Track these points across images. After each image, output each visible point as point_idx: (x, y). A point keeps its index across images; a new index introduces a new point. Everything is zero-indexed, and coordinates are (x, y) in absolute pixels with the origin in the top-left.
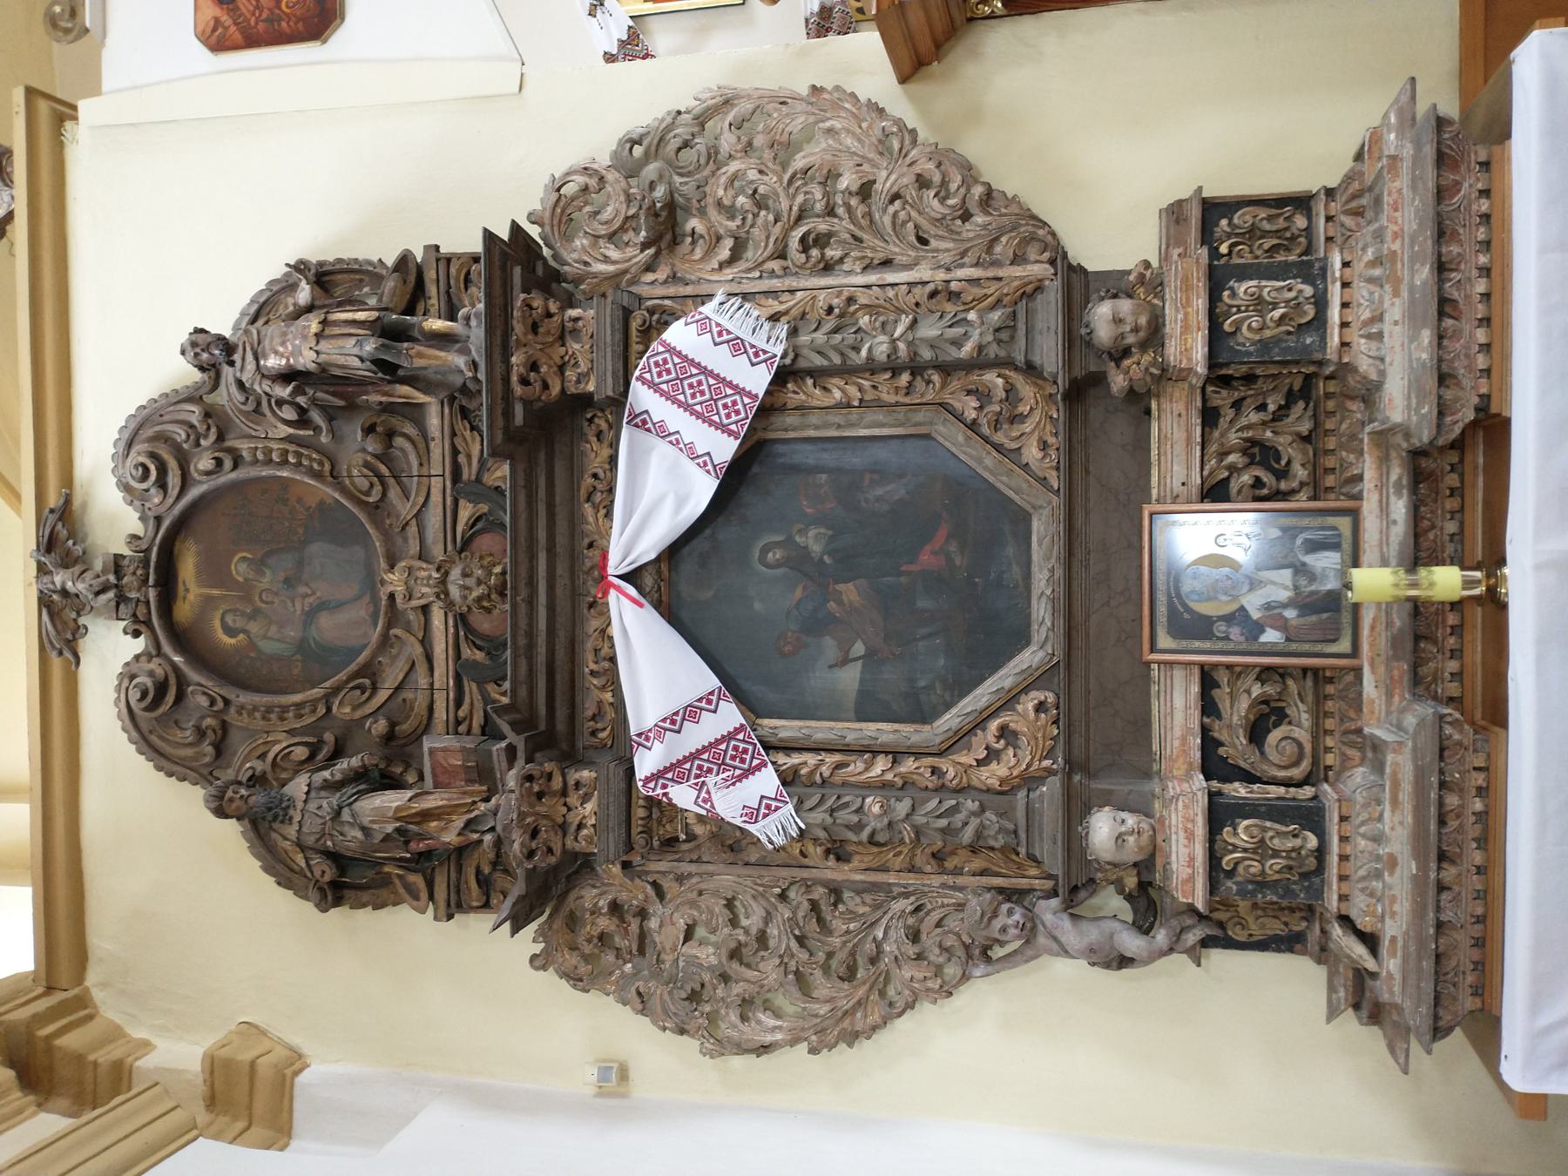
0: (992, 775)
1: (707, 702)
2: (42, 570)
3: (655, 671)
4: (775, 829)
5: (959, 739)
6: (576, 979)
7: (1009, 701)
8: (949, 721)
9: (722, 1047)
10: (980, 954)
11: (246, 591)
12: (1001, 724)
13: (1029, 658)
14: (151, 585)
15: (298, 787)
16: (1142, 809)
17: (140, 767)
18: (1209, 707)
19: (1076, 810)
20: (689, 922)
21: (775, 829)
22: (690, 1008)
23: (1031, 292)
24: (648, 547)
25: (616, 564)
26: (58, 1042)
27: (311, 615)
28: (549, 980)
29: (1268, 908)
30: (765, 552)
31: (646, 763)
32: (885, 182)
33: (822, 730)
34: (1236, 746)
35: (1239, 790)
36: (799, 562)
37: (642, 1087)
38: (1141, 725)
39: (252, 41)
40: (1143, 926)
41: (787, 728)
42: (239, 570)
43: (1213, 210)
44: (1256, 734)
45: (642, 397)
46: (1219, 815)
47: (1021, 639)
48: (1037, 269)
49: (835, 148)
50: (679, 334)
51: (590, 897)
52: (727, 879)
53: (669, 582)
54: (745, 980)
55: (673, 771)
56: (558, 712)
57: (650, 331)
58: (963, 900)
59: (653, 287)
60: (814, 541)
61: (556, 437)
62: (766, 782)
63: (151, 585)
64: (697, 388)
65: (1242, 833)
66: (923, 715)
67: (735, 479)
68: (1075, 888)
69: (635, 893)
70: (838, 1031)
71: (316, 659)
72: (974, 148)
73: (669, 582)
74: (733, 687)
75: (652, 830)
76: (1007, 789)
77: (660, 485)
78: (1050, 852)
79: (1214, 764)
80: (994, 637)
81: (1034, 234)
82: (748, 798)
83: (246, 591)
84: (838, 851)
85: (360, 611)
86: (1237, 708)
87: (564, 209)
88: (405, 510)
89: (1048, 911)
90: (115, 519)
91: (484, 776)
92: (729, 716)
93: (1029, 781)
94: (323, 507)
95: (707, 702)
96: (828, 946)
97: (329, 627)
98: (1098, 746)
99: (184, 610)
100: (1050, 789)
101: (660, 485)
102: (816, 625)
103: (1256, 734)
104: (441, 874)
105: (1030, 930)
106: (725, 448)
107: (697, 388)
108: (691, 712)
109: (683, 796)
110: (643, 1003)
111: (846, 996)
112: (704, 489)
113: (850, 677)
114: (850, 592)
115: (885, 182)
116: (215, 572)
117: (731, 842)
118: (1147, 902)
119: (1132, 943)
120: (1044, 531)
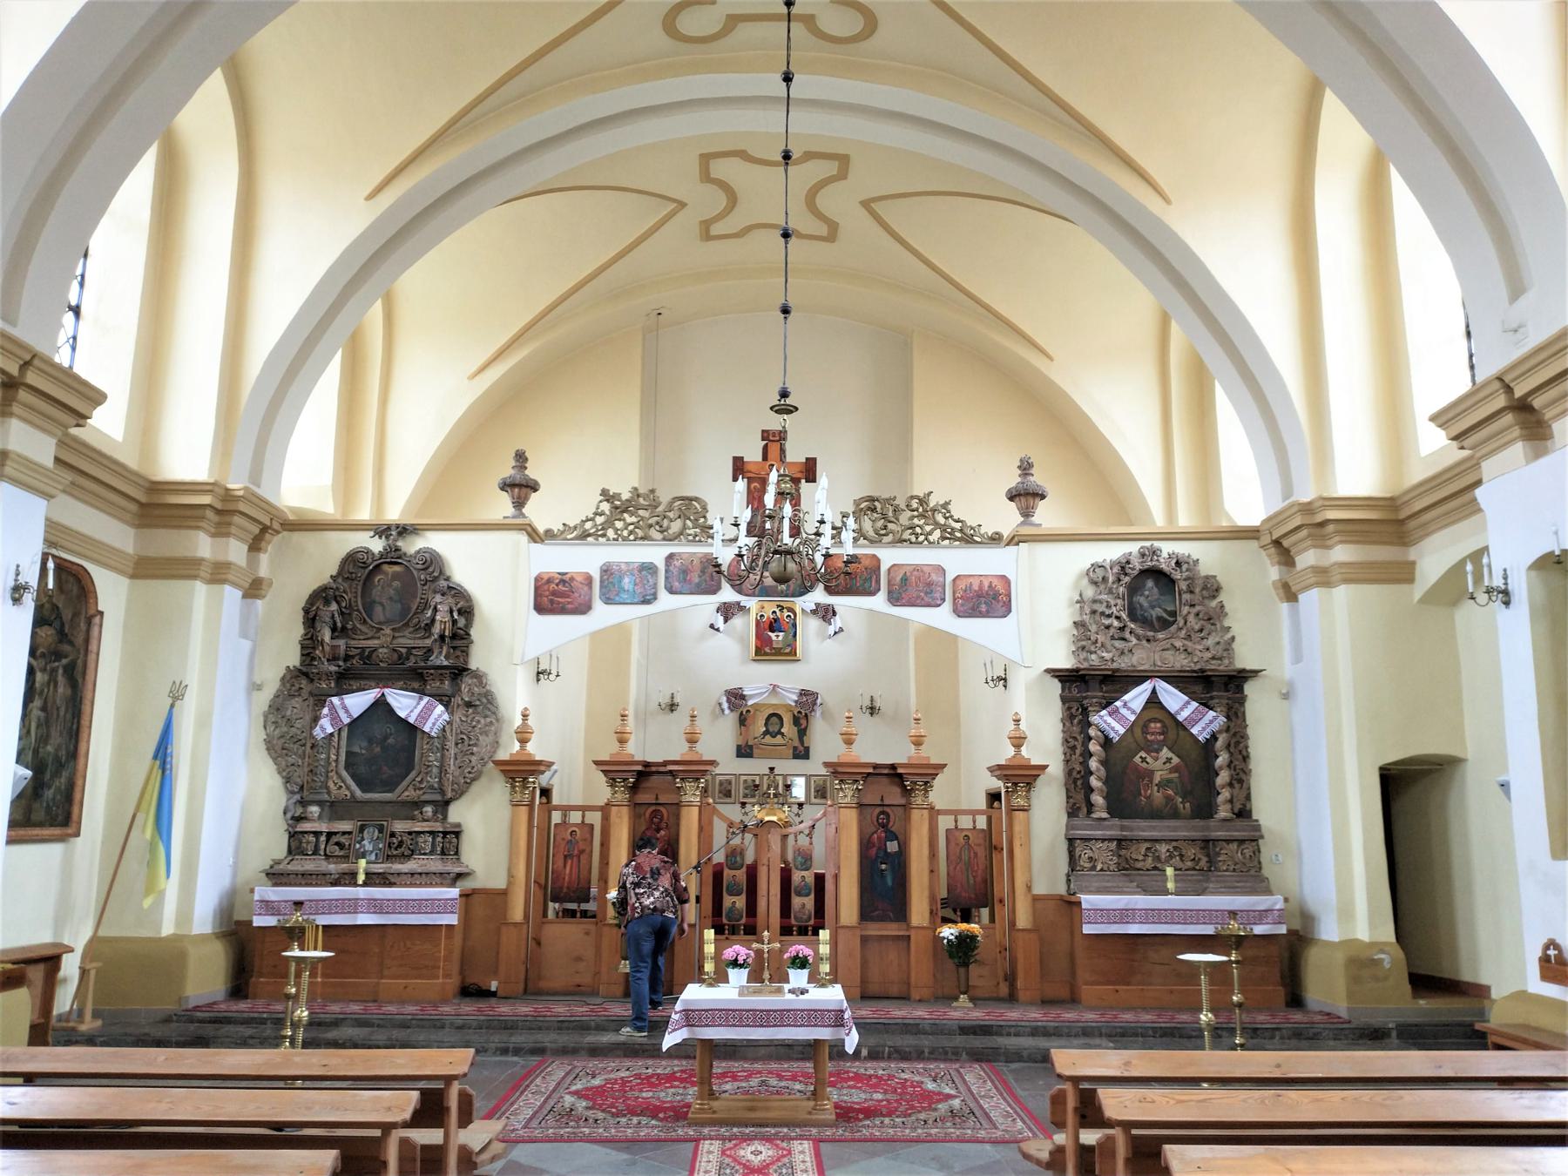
0: (331, 784)
1: (350, 715)
2: (398, 526)
3: (357, 702)
4: (318, 733)
5: (340, 777)
6: (283, 679)
7: (348, 788)
8: (345, 774)
9: (266, 717)
10: (287, 780)
11: (390, 586)
12: (344, 786)
13: (358, 793)
14: (393, 556)
15: (334, 607)
16: (320, 817)
17: (342, 553)
18: (344, 833)
19: (320, 803)
20: (296, 707)
21: (318, 733)
22: (276, 707)
23: (443, 792)
24: (390, 700)
25: (387, 691)
26: (215, 85)
27: (382, 604)
28: (282, 672)
29: (296, 843)
30: (391, 728)
31: (335, 700)
32: (474, 759)
33: (344, 742)
34: (335, 839)
35: (323, 838)
36: (386, 738)
37: (255, 693)
38: (342, 819)
39: (536, 589)
40: (293, 818)
41: (345, 734)
42: (396, 584)
43: (457, 834)
44: (337, 844)
45: (426, 699)
46: (317, 834)
47: (364, 791)
48: (449, 795)
49: (482, 749)
50: (440, 708)
51: (304, 682)
52: (308, 717)
53: (381, 705)
54: (282, 722)
55: (332, 707)
56: (346, 681)
57: (441, 702)
58: (300, 775)
59: (457, 700)
60: (391, 741)
61: (416, 677)
62: (330, 730)
63: (393, 556)
64: (425, 715)
65: (312, 838)
66: (347, 768)
67: (404, 721)
68: (303, 803)
69: (305, 694)
70: (270, 746)
71: (369, 607)
72: (483, 780)
73: (381, 705)
74: (354, 722)
75: (320, 700)
76: (327, 788)
77: (405, 703)
78: (312, 797)
79: (330, 835)
80: (365, 785)
81: (459, 794)
82: (326, 726)
83: (390, 586)
84: (313, 747)
85: (382, 619)
86: (343, 839)
87: (479, 676)
88: (406, 633)
89: (297, 797)
90: (413, 546)
91: (333, 659)
92: (346, 721)
93: (329, 793)
94: (409, 609)
95: (350, 715)
96: (287, 741)
97: (378, 609)
98: (335, 809)
99: (385, 567)
100: (326, 797)
101: (405, 703)
102: (370, 741)
103: (337, 844)
104: (309, 645)
105: (293, 793)
106: (411, 720)
107: (425, 715)
108: (347, 711)
109: (325, 711)
110: (277, 696)
111: (278, 748)
112: (402, 714)
113: (356, 749)
114: (378, 750)
115: (474, 759)
116: (396, 576)
117: (316, 719)
118: (299, 819)
119: (289, 815)
120: (388, 796)
